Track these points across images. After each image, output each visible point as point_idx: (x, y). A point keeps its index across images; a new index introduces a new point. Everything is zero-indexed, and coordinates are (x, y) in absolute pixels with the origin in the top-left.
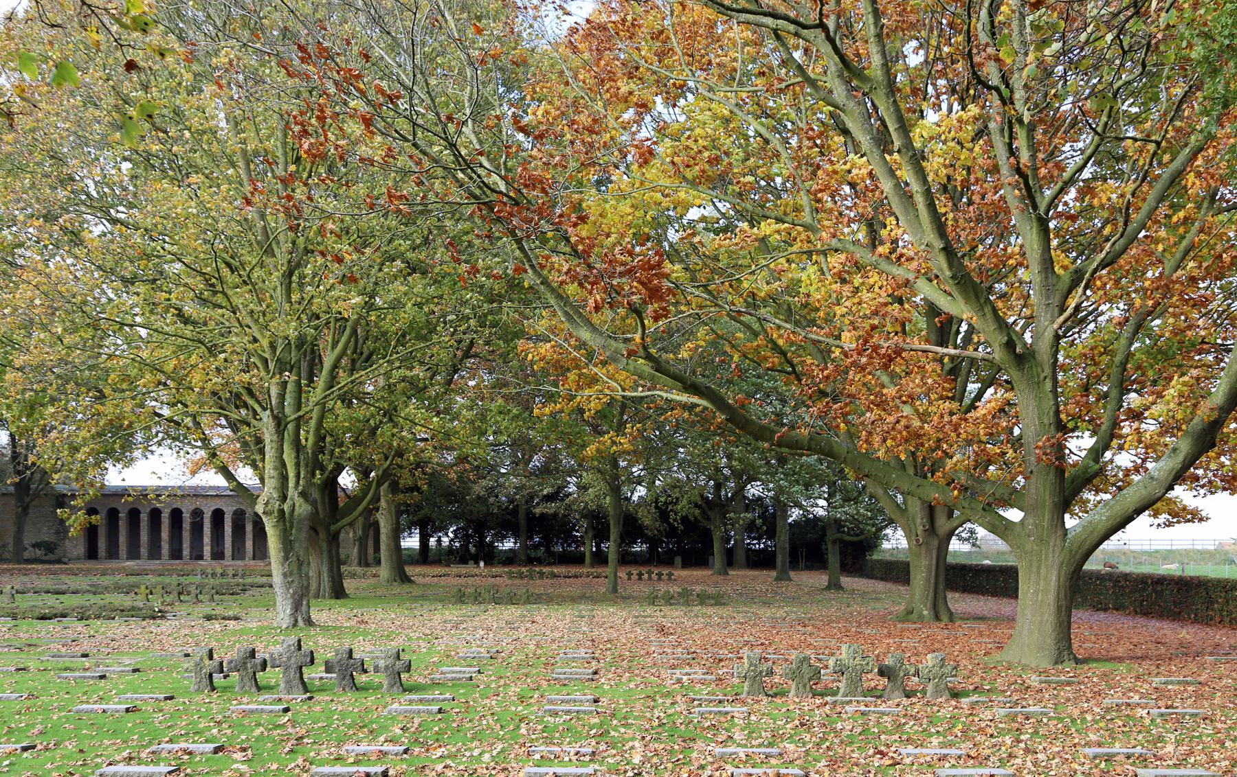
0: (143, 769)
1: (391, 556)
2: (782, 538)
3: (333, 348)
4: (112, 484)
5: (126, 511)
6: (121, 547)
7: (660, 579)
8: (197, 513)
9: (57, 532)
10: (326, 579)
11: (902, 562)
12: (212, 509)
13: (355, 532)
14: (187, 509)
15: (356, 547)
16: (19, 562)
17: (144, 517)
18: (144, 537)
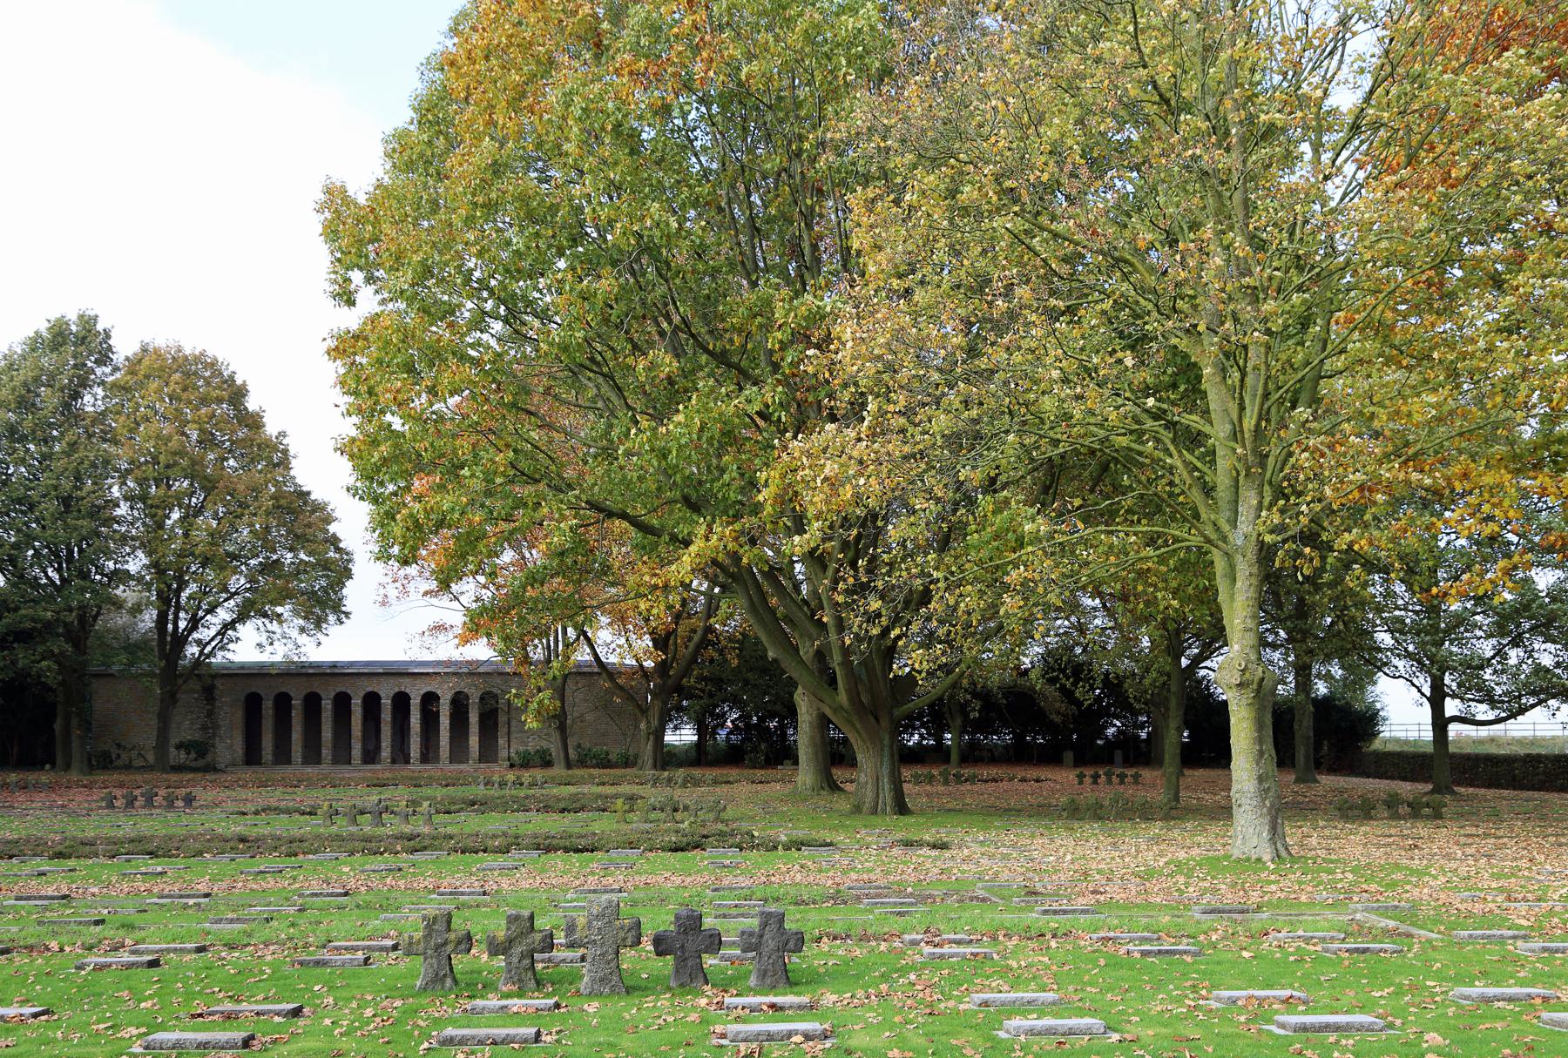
0: (73, 1052)
1: (816, 753)
2: (1305, 724)
3: (1171, 456)
4: (311, 660)
5: (302, 697)
6: (294, 748)
7: (1122, 782)
8: (401, 700)
9: (204, 728)
10: (887, 787)
11: (261, 758)
12: (422, 692)
13: (649, 722)
14: (386, 692)
15: (650, 743)
16: (164, 770)
17: (268, 707)
18: (327, 733)
